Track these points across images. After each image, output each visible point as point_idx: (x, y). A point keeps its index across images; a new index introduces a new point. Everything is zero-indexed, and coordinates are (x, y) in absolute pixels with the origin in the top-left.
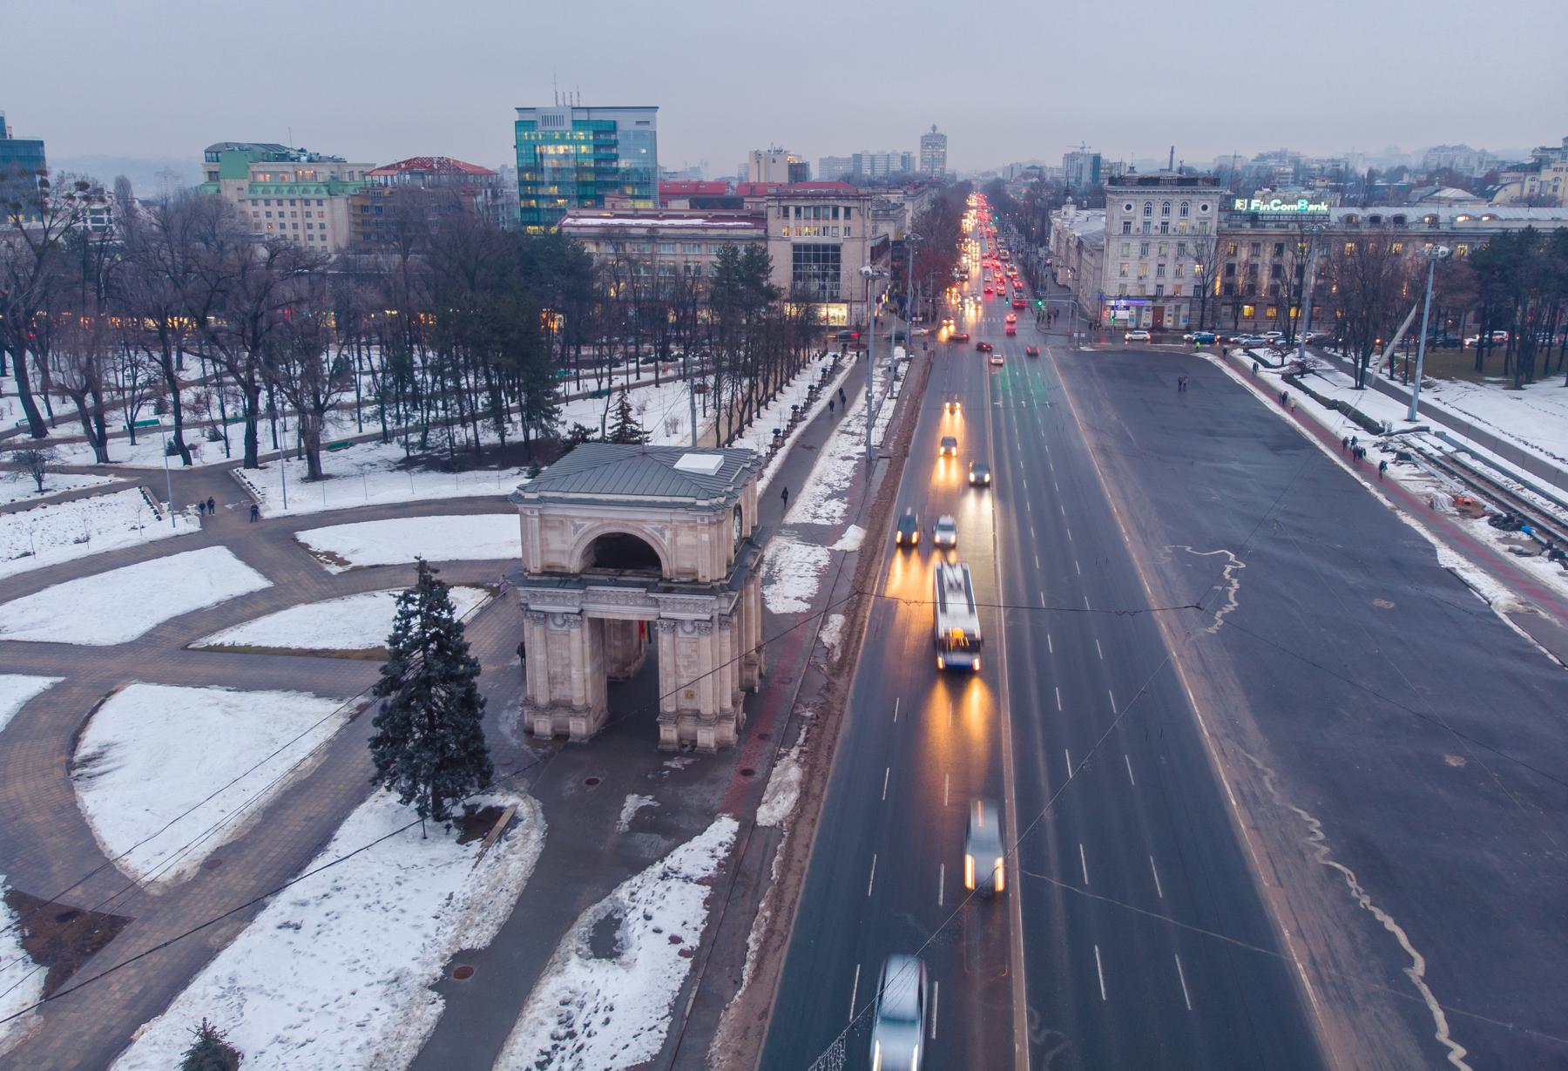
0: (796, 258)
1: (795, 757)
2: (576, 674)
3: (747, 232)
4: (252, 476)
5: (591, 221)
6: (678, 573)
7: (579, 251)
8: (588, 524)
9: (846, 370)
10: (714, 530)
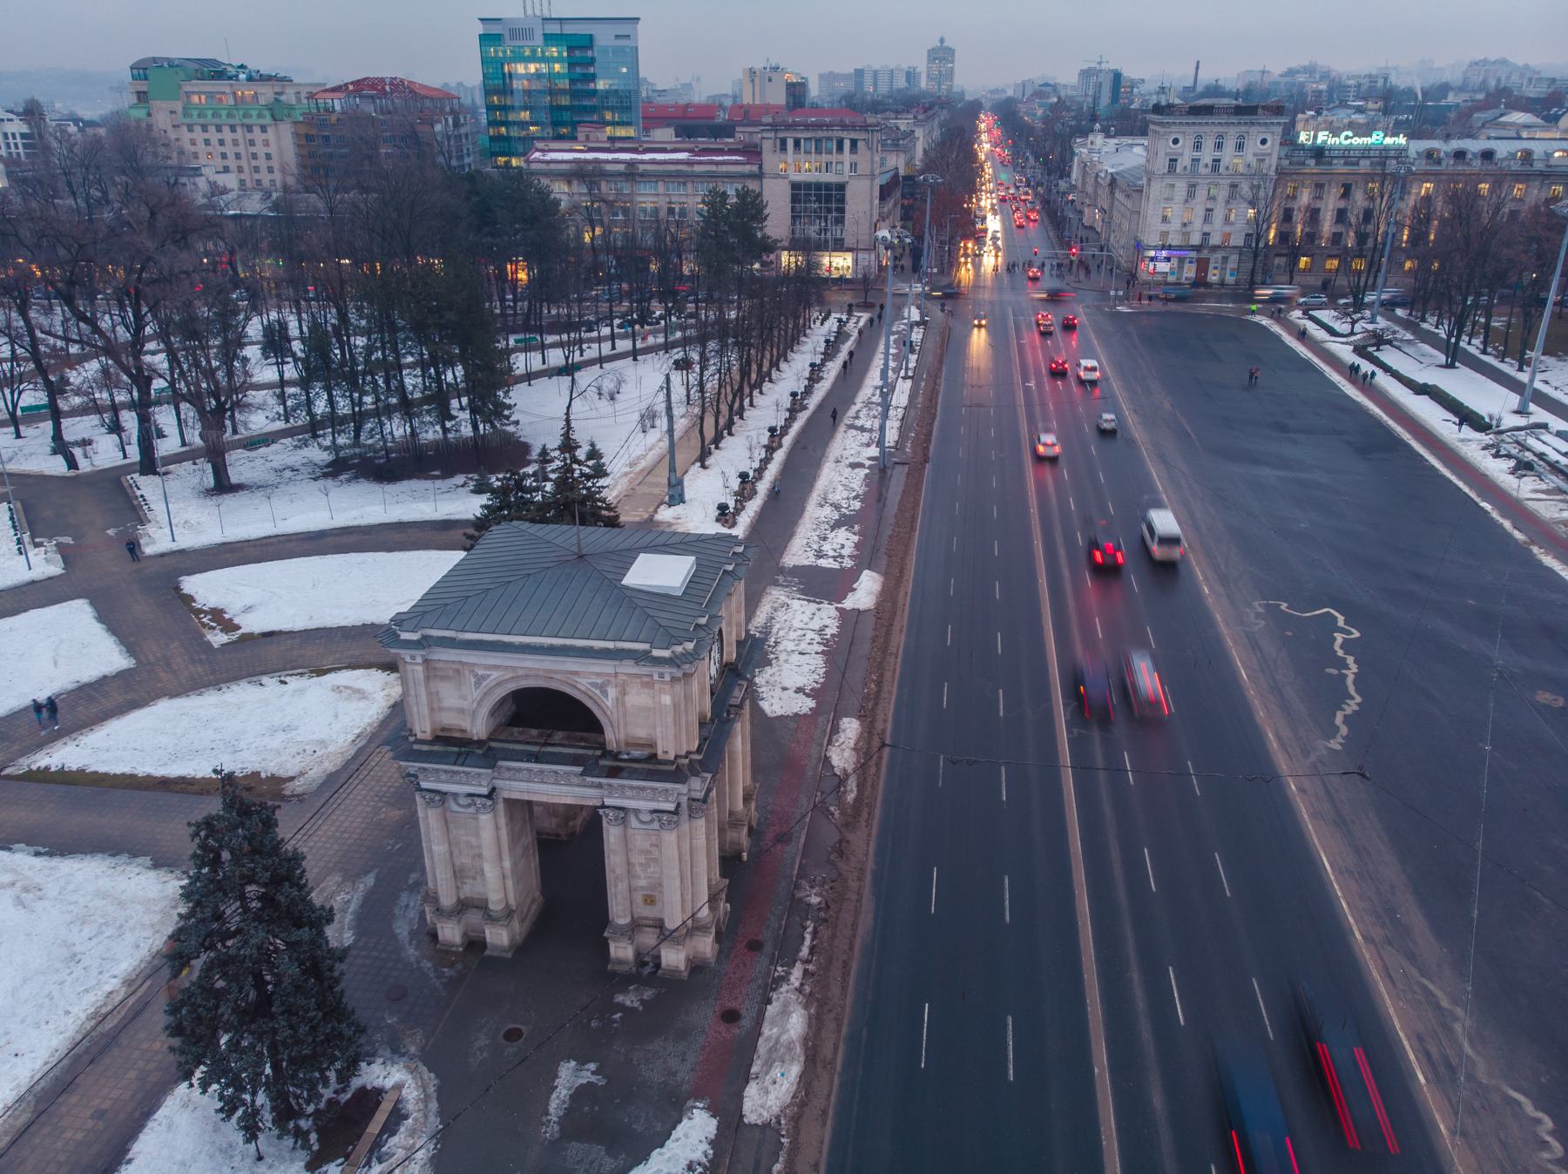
0: (795, 199)
1: (797, 984)
2: (491, 872)
3: (739, 169)
4: (147, 487)
5: (563, 155)
6: (628, 744)
7: (544, 194)
8: (495, 674)
9: (852, 339)
10: (679, 688)
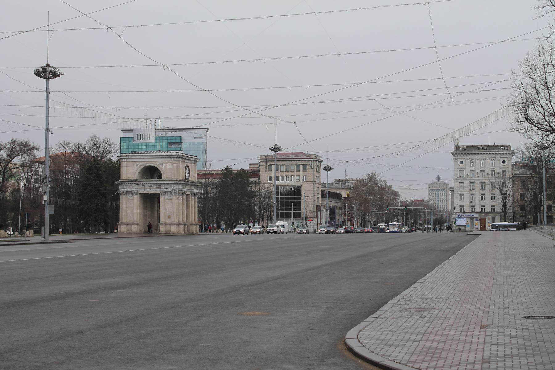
8: (141, 164)
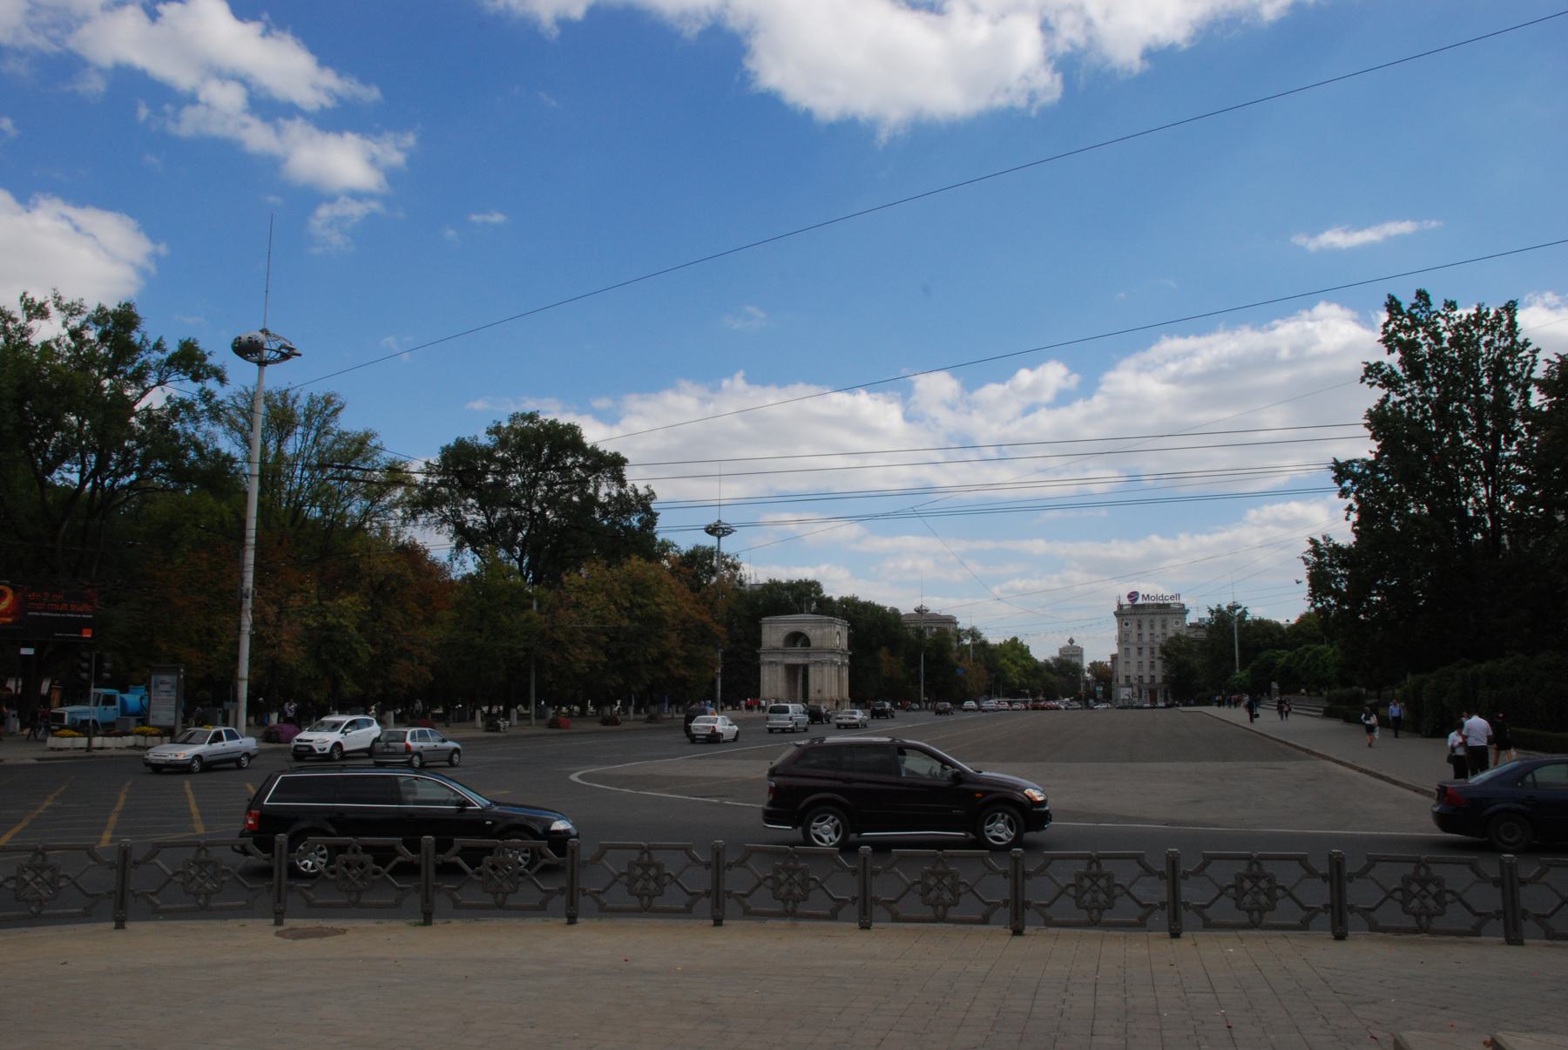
8: (786, 629)
